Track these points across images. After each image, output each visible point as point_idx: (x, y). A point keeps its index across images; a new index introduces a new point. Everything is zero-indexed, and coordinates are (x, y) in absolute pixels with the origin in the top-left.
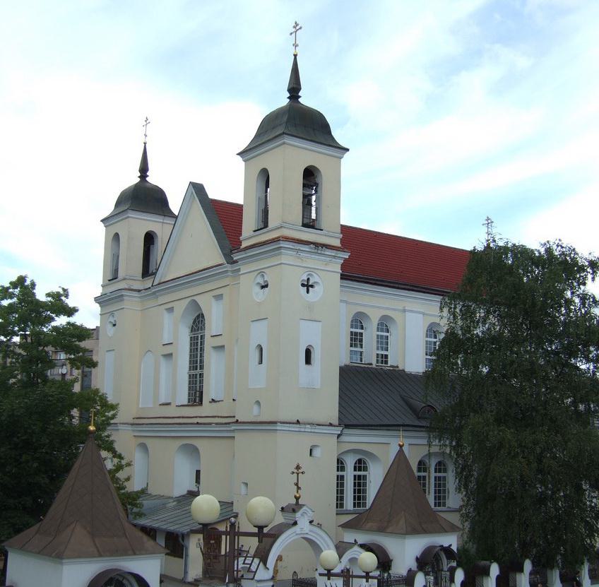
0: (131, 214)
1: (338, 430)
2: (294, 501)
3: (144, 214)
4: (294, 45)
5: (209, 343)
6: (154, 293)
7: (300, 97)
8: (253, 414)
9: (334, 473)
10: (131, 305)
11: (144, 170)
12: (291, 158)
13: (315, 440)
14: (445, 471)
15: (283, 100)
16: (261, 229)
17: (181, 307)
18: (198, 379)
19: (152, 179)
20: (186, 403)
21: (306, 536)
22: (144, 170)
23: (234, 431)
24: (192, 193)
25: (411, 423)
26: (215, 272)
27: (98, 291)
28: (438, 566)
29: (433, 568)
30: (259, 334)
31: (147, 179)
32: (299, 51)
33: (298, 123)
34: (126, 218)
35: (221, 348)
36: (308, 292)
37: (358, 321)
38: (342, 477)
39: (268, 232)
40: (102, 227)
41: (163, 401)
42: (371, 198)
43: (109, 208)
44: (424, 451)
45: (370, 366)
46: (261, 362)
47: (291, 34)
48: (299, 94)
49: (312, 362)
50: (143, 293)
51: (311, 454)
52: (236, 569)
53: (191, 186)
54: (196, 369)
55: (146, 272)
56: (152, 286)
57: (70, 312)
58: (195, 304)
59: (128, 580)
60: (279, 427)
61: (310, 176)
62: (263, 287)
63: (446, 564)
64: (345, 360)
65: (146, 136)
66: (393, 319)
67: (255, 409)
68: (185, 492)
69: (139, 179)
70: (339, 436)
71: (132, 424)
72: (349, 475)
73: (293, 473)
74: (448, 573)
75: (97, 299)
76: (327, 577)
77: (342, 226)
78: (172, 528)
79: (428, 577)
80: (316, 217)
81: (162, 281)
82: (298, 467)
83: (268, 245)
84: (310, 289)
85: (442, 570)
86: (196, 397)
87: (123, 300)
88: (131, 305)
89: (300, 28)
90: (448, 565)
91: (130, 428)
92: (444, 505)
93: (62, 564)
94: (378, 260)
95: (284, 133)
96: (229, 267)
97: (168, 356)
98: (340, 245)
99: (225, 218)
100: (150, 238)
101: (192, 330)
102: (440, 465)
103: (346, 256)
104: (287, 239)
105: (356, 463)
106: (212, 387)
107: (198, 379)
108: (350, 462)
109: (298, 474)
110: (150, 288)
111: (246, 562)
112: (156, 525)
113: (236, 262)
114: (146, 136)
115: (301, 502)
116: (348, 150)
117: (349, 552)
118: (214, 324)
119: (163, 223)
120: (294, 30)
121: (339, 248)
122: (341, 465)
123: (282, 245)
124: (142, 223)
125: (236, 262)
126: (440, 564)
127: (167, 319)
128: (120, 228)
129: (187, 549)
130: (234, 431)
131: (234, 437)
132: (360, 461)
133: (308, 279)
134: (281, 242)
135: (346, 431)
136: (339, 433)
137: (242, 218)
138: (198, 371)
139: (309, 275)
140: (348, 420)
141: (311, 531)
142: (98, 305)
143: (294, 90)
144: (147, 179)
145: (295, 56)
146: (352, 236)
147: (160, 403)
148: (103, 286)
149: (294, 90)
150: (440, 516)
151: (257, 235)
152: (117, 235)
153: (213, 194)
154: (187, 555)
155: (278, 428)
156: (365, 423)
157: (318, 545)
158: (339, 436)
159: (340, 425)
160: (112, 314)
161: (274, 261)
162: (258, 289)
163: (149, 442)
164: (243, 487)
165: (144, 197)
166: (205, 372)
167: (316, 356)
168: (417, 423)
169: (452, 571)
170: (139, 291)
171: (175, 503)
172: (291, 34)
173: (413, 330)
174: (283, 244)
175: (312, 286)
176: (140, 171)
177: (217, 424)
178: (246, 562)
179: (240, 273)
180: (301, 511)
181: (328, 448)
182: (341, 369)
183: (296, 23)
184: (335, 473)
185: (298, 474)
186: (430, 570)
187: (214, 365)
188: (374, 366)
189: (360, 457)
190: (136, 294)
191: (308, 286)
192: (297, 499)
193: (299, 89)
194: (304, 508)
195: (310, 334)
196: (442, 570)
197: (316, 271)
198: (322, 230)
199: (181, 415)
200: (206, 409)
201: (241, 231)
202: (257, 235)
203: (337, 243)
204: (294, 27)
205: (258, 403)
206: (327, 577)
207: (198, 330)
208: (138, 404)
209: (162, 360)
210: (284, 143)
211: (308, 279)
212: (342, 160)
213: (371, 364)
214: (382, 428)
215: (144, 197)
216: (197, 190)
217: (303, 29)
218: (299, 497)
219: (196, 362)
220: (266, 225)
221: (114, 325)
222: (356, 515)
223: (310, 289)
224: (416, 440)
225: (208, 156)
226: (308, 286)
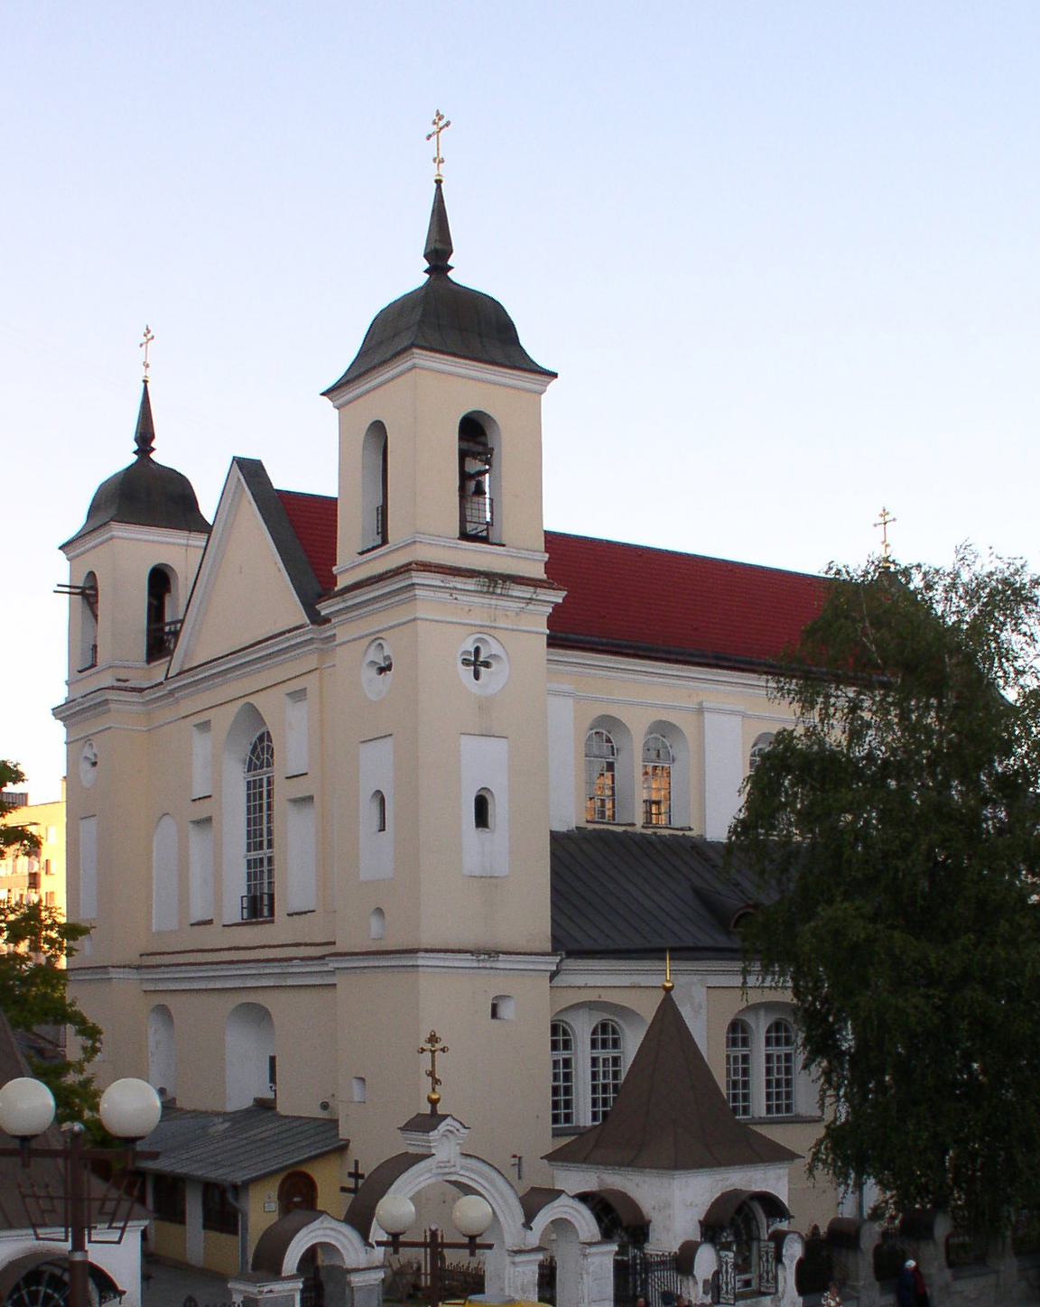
1: (551, 963)
2: (427, 1109)
3: (138, 528)
4: (435, 160)
5: (282, 791)
6: (171, 693)
7: (451, 268)
8: (373, 933)
10: (125, 711)
11: (145, 437)
12: (442, 387)
13: (498, 985)
16: (374, 548)
17: (224, 719)
18: (265, 868)
19: (465, 272)
20: (239, 920)
21: (453, 1178)
22: (145, 437)
23: (332, 973)
24: (239, 480)
25: (707, 941)
26: (299, 640)
27: (60, 695)
29: (737, 1235)
30: (376, 767)
31: (152, 456)
32: (151, 374)
33: (449, 320)
34: (410, 370)
36: (477, 676)
38: (567, 1063)
39: (98, 672)
40: (328, 413)
41: (198, 915)
42: (601, 476)
43: (76, 520)
44: (732, 1006)
45: (629, 829)
46: (382, 829)
47: (429, 137)
48: (450, 263)
49: (490, 820)
50: (148, 695)
52: (429, 1277)
53: (235, 462)
54: (261, 848)
55: (159, 642)
56: (166, 678)
58: (253, 715)
60: (422, 960)
62: (382, 670)
64: (569, 813)
65: (147, 366)
67: (375, 925)
68: (248, 1103)
69: (135, 458)
70: (553, 975)
71: (139, 967)
73: (423, 1050)
74: (772, 1245)
75: (57, 712)
76: (467, 1251)
77: (547, 533)
78: (213, 1174)
79: (723, 1253)
80: (492, 518)
81: (186, 668)
83: (388, 581)
84: (482, 669)
85: (759, 1240)
86: (259, 906)
87: (108, 704)
89: (447, 124)
90: (768, 1227)
91: (134, 975)
92: (789, 1108)
94: (625, 602)
95: (413, 345)
96: (311, 631)
98: (545, 577)
99: (302, 527)
100: (160, 580)
101: (251, 767)
102: (604, 1031)
103: (558, 597)
104: (427, 567)
105: (594, 1033)
106: (296, 883)
107: (265, 868)
108: (582, 1029)
109: (433, 1052)
110: (161, 683)
112: (184, 1170)
113: (326, 620)
115: (441, 1110)
116: (555, 375)
118: (292, 753)
119: (188, 546)
120: (435, 128)
121: (540, 581)
122: (560, 1036)
124: (141, 547)
125: (326, 620)
126: (754, 1228)
127: (201, 746)
128: (96, 560)
129: (245, 1215)
130: (332, 973)
131: (335, 985)
132: (604, 1027)
133: (477, 650)
134: (414, 573)
135: (571, 964)
136: (554, 968)
138: (265, 852)
141: (462, 1168)
142: (60, 723)
144: (152, 456)
145: (439, 182)
146: (573, 559)
147: (193, 922)
150: (751, 1130)
151: (367, 562)
152: (378, 430)
153: (282, 479)
154: (245, 1229)
155: (420, 962)
156: (613, 946)
158: (553, 975)
159: (554, 952)
160: (87, 740)
163: (168, 1001)
164: (356, 1085)
165: (147, 494)
166: (276, 852)
167: (498, 811)
168: (723, 941)
170: (141, 690)
171: (227, 1125)
172: (429, 137)
173: (716, 741)
174: (418, 578)
175: (487, 665)
176: (426, 256)
177: (302, 959)
179: (336, 643)
180: (443, 1127)
181: (531, 998)
182: (555, 837)
183: (438, 114)
184: (547, 1056)
185: (433, 1052)
187: (296, 837)
188: (638, 829)
189: (606, 1016)
190: (134, 697)
191: (477, 663)
192: (434, 1103)
193: (448, 252)
194: (449, 1120)
195: (483, 763)
197: (492, 632)
198: (504, 545)
199: (233, 945)
200: (279, 931)
202: (367, 562)
203: (539, 572)
204: (145, 335)
206: (467, 1251)
207: (261, 767)
210: (414, 367)
211: (477, 650)
212: (543, 396)
213: (633, 825)
215: (147, 494)
216: (250, 472)
218: (438, 1100)
219: (259, 833)
220: (385, 541)
221: (94, 764)
222: (573, 1138)
224: (731, 977)
225: (266, 407)
226: (477, 663)
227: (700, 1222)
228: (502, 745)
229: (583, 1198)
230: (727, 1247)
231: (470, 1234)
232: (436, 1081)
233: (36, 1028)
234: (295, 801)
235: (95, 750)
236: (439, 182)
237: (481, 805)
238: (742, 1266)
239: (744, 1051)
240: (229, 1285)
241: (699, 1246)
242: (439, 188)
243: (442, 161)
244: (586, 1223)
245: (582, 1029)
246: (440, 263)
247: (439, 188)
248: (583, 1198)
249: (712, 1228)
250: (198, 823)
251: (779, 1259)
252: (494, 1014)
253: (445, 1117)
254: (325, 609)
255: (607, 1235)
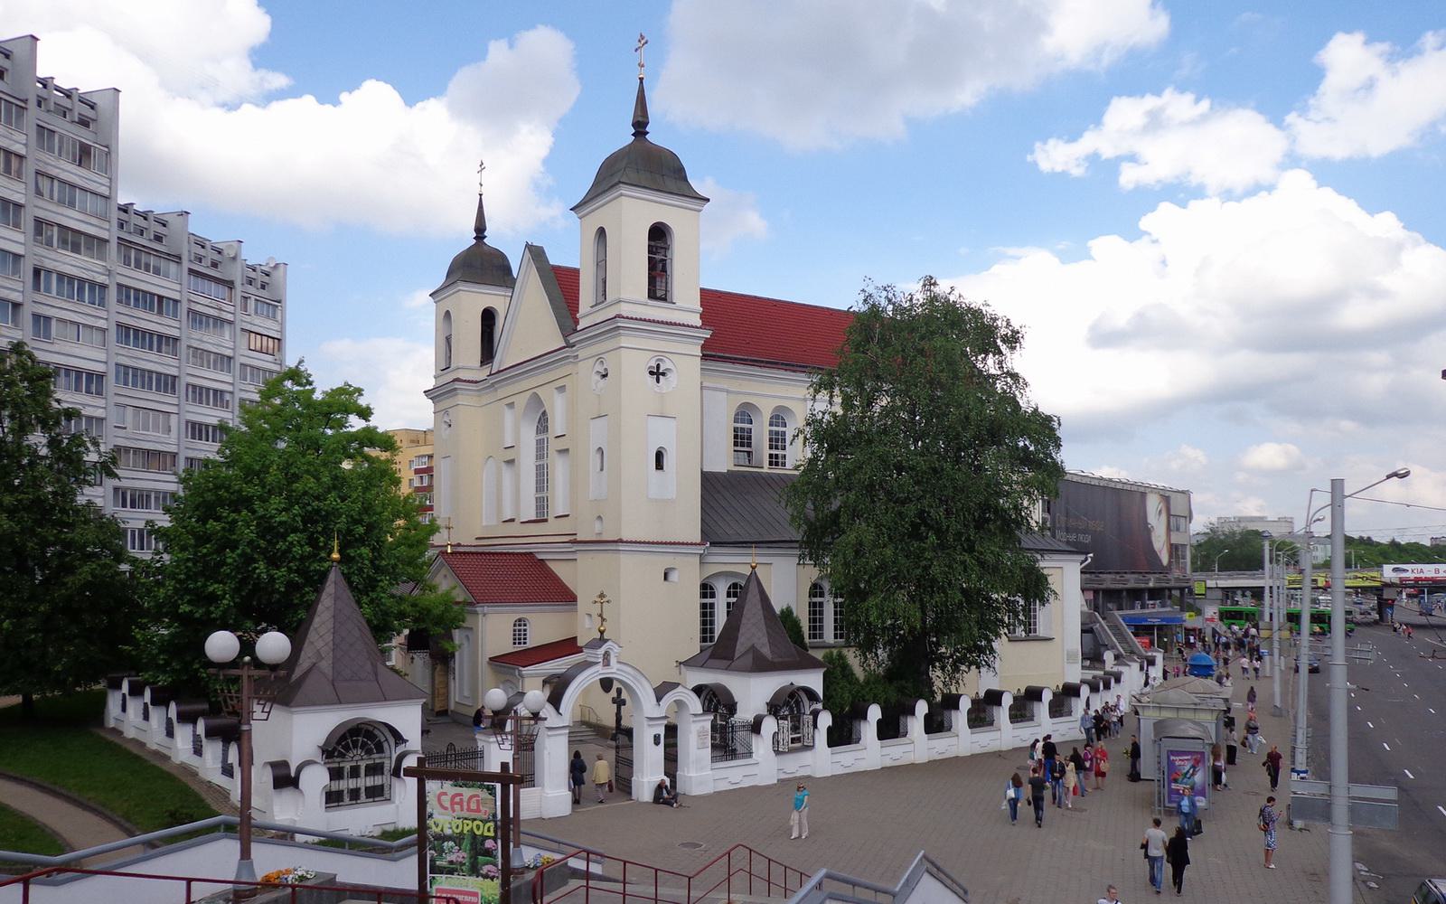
0: (462, 286)
2: (598, 635)
5: (554, 445)
9: (696, 601)
12: (635, 212)
14: (822, 595)
15: (626, 137)
17: (522, 401)
28: (799, 710)
29: (791, 710)
30: (596, 434)
31: (485, 240)
35: (565, 451)
36: (658, 381)
37: (745, 413)
43: (440, 279)
46: (602, 470)
51: (666, 578)
55: (488, 353)
57: (365, 413)
59: (379, 730)
61: (659, 234)
62: (604, 376)
63: (807, 707)
65: (481, 185)
66: (794, 415)
67: (597, 527)
72: (720, 602)
73: (596, 602)
74: (811, 717)
77: (703, 291)
82: (602, 596)
84: (661, 377)
85: (804, 714)
88: (466, 401)
89: (646, 43)
93: (292, 713)
94: (744, 331)
95: (620, 182)
97: (510, 462)
99: (563, 285)
100: (488, 317)
101: (538, 432)
103: (707, 334)
105: (729, 588)
106: (559, 505)
111: (265, 710)
114: (481, 185)
115: (606, 636)
116: (708, 200)
117: (668, 695)
118: (557, 425)
122: (707, 590)
123: (619, 324)
124: (474, 299)
127: (509, 416)
128: (448, 304)
131: (576, 560)
137: (578, 294)
139: (658, 360)
140: (713, 536)
141: (618, 670)
143: (640, 127)
148: (435, 377)
149: (640, 127)
152: (448, 314)
157: (589, 685)
161: (610, 344)
162: (598, 377)
169: (815, 714)
170: (476, 382)
172: (636, 50)
175: (663, 374)
178: (265, 710)
181: (689, 575)
186: (787, 713)
187: (559, 470)
191: (657, 373)
192: (602, 633)
194: (609, 643)
195: (663, 434)
196: (804, 714)
197: (667, 355)
200: (552, 527)
201: (578, 308)
204: (639, 41)
205: (600, 518)
208: (482, 522)
209: (504, 466)
210: (621, 195)
211: (658, 366)
214: (761, 545)
216: (536, 254)
217: (634, 49)
223: (661, 377)
227: (767, 704)
228: (672, 423)
229: (698, 690)
230: (784, 718)
231: (1141, 782)
232: (603, 620)
233: (1165, 561)
234: (560, 452)
235: (605, 366)
236: (641, 79)
237: (659, 456)
238: (795, 729)
239: (705, 601)
240: (477, 737)
241: (240, 651)
242: (481, 199)
243: (643, 66)
244: (695, 704)
245: (721, 588)
246: (641, 130)
247: (481, 199)
248: (698, 690)
249: (774, 708)
250: (560, 452)
251: (815, 726)
252: (666, 578)
253: (608, 640)
254: (573, 339)
255: (706, 711)
